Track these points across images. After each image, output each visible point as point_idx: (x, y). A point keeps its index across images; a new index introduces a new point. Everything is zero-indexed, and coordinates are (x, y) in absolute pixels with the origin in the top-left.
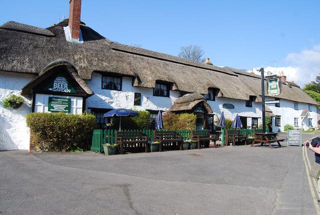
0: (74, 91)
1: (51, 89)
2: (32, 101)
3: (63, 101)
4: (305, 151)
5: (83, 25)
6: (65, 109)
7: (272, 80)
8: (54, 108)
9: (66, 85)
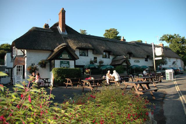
1: (61, 58)
9: (67, 55)
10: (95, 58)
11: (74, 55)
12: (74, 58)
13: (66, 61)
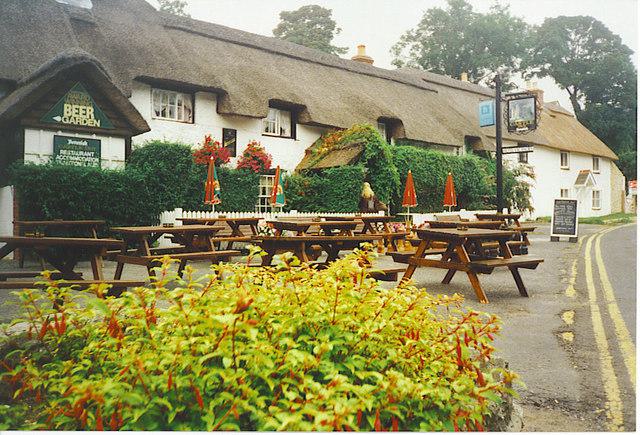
1: (58, 119)
4: (600, 292)
7: (404, 403)
9: (90, 110)
10: (229, 135)
11: (127, 113)
12: (126, 124)
13: (84, 140)
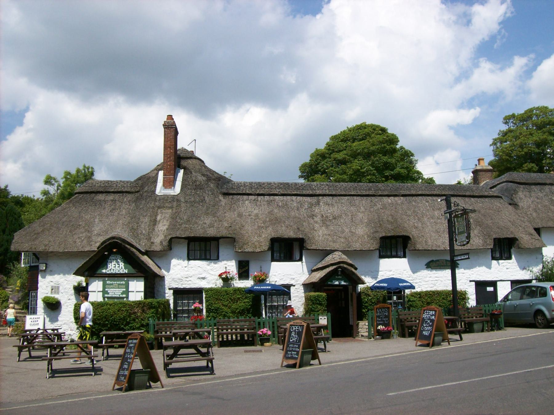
0: (133, 271)
1: (104, 271)
2: (294, 243)
3: (119, 284)
5: (353, 270)
6: (122, 294)
8: (108, 294)
